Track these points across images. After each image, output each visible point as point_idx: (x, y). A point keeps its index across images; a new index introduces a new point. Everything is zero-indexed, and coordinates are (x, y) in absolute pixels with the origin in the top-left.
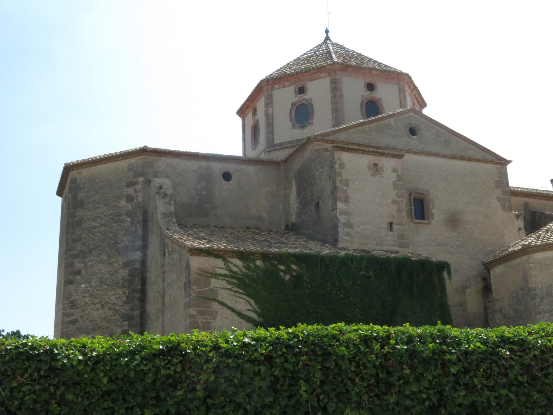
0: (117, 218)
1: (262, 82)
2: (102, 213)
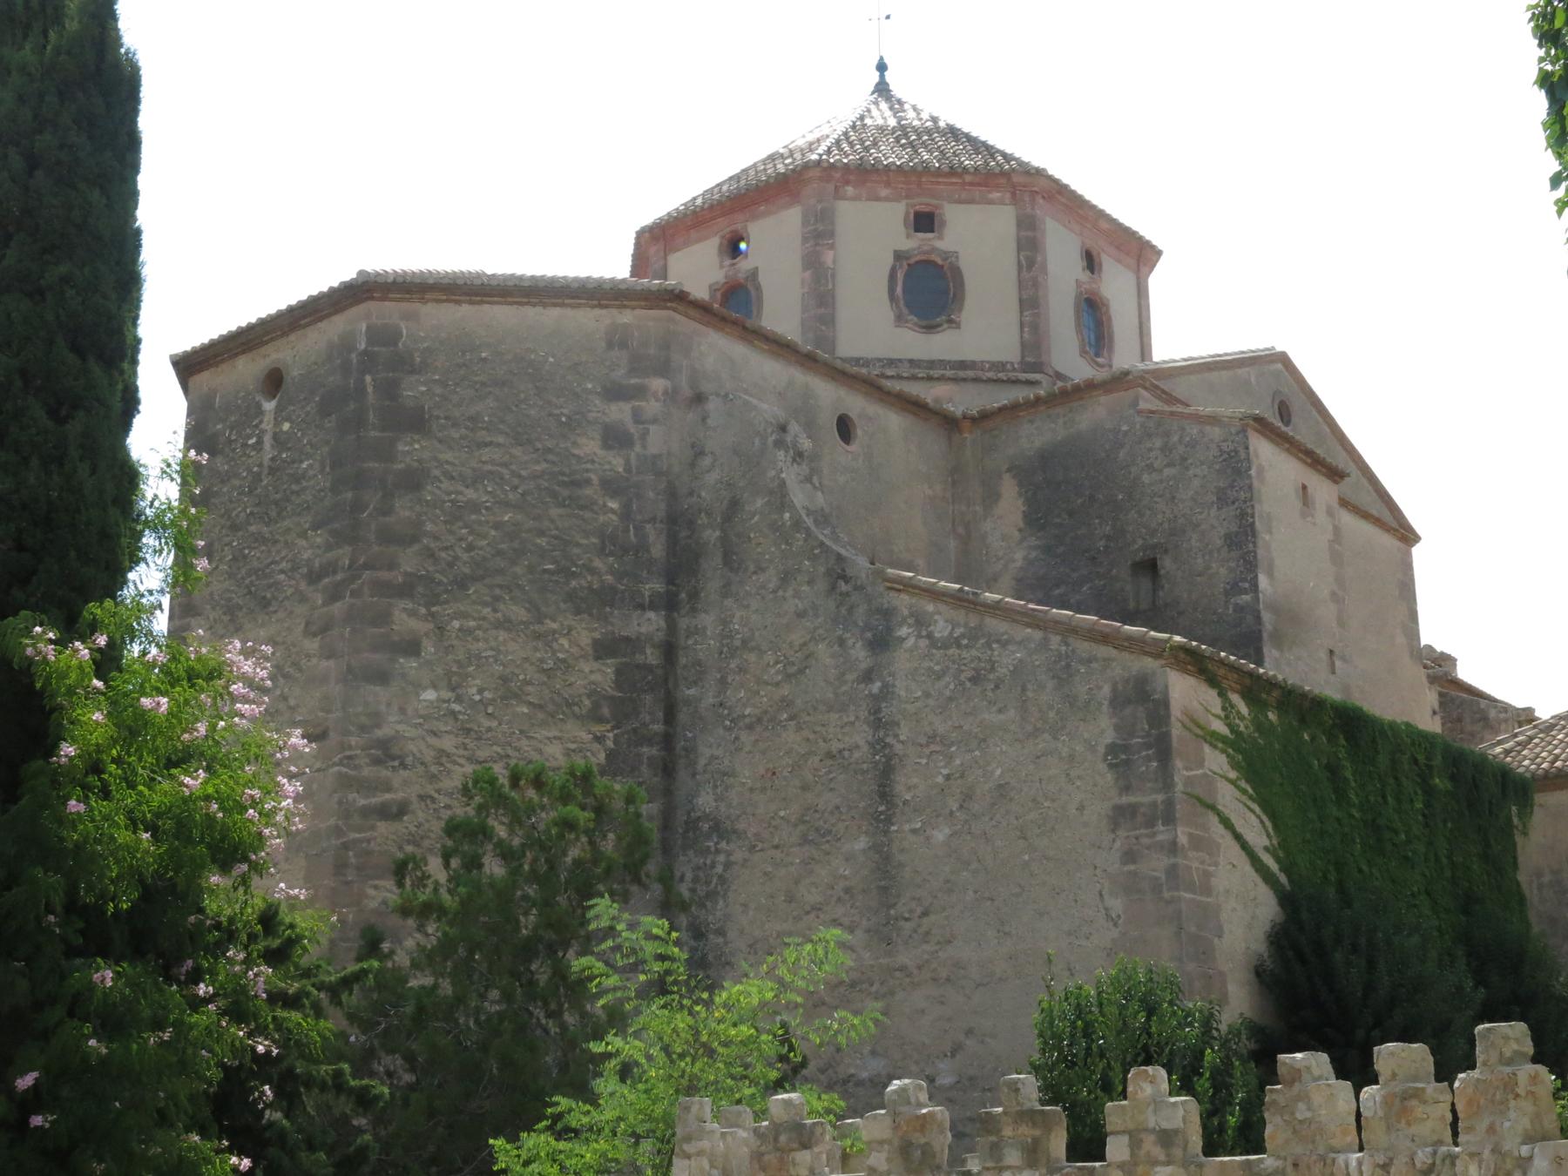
0: (566, 493)
2: (505, 465)
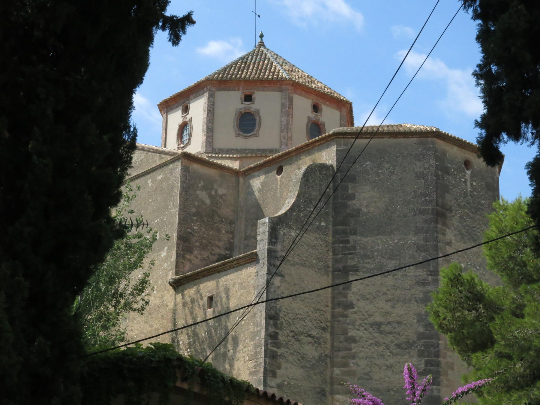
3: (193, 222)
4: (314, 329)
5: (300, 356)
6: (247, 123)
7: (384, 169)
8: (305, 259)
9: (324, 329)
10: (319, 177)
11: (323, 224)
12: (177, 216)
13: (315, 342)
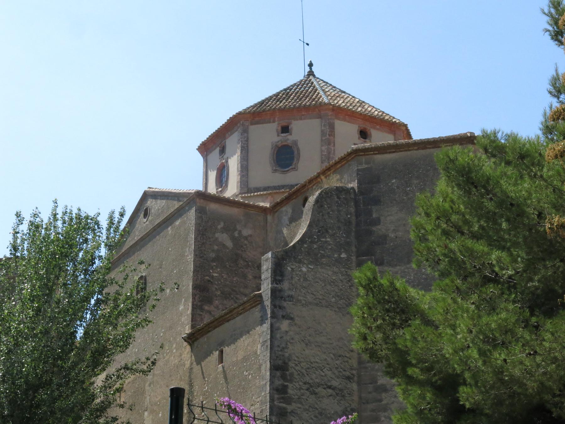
1: (239, 114)
3: (212, 268)
4: (336, 379)
5: (317, 412)
6: (285, 157)
7: (413, 186)
8: (321, 297)
9: (348, 378)
10: (337, 202)
11: (343, 255)
12: (192, 263)
13: (337, 394)
